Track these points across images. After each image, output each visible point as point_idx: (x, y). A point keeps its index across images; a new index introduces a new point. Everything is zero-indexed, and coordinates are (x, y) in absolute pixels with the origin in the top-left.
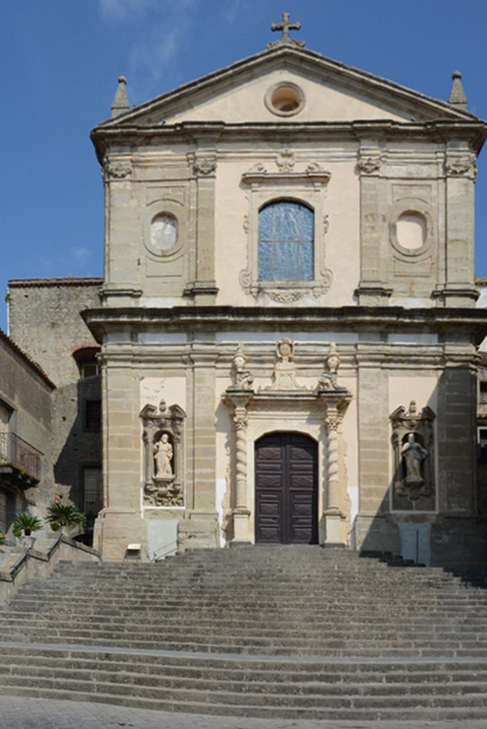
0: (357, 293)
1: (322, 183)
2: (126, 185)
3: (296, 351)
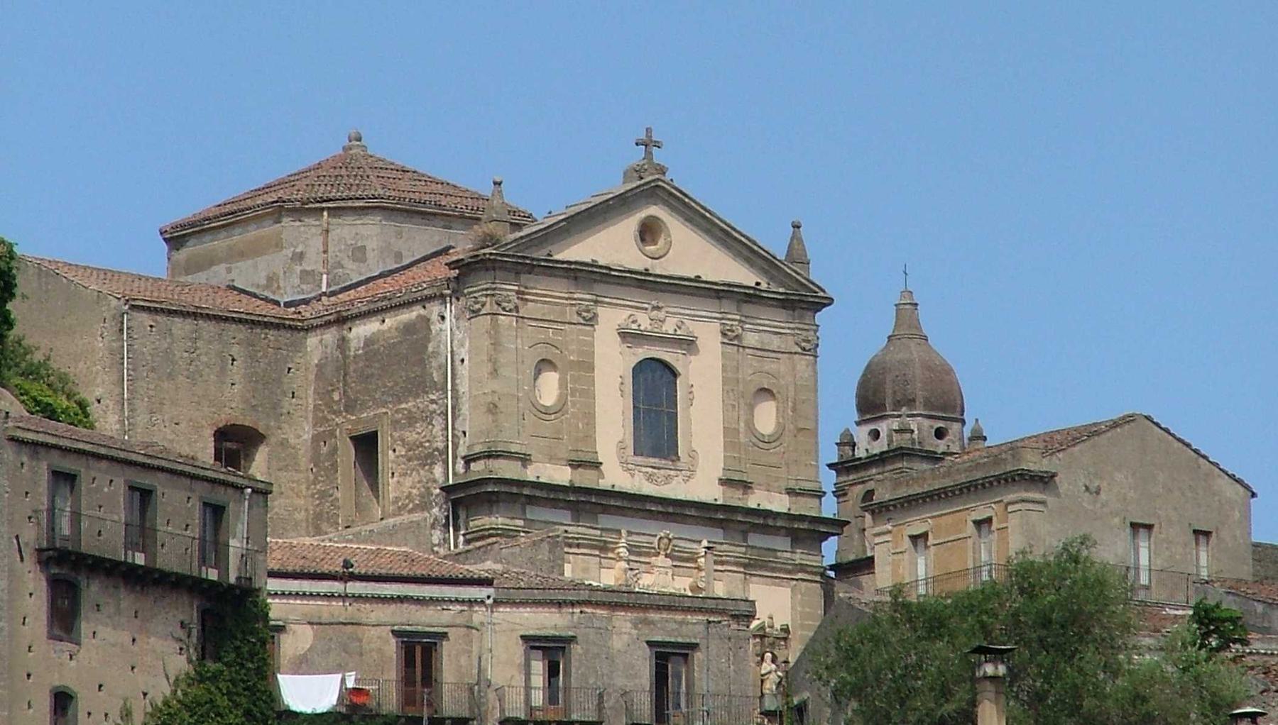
0: (726, 482)
1: (688, 345)
2: (513, 321)
3: (674, 546)
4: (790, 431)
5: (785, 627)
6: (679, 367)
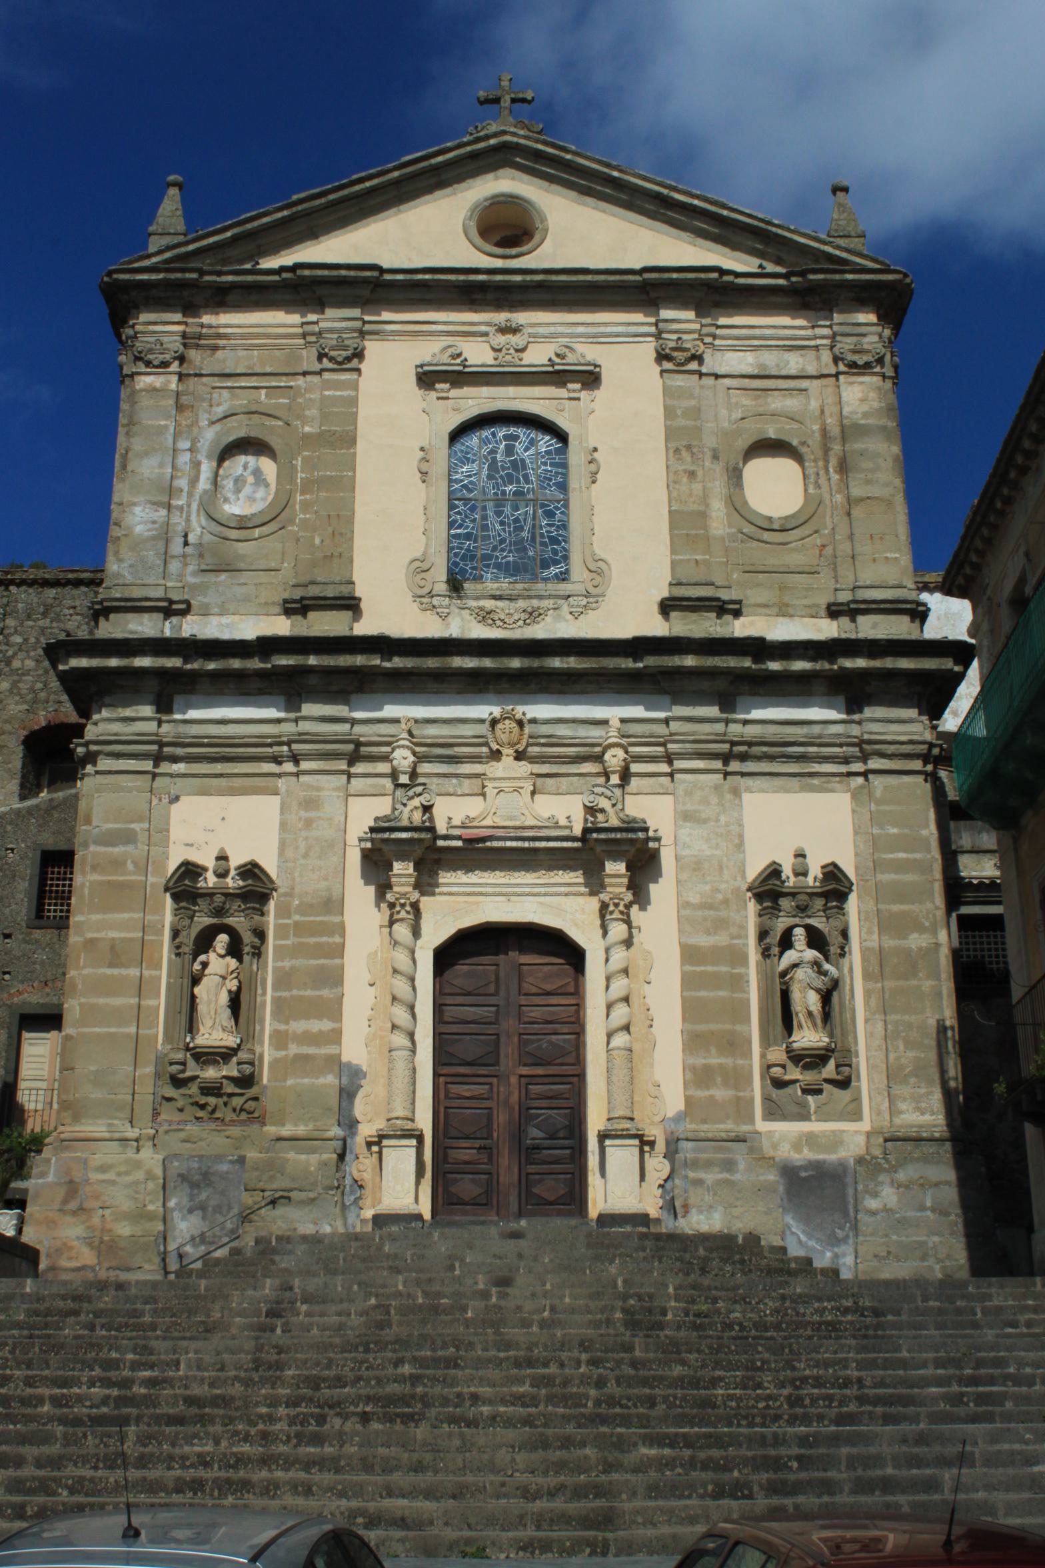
0: (667, 607)
5: (831, 868)
6: (563, 422)
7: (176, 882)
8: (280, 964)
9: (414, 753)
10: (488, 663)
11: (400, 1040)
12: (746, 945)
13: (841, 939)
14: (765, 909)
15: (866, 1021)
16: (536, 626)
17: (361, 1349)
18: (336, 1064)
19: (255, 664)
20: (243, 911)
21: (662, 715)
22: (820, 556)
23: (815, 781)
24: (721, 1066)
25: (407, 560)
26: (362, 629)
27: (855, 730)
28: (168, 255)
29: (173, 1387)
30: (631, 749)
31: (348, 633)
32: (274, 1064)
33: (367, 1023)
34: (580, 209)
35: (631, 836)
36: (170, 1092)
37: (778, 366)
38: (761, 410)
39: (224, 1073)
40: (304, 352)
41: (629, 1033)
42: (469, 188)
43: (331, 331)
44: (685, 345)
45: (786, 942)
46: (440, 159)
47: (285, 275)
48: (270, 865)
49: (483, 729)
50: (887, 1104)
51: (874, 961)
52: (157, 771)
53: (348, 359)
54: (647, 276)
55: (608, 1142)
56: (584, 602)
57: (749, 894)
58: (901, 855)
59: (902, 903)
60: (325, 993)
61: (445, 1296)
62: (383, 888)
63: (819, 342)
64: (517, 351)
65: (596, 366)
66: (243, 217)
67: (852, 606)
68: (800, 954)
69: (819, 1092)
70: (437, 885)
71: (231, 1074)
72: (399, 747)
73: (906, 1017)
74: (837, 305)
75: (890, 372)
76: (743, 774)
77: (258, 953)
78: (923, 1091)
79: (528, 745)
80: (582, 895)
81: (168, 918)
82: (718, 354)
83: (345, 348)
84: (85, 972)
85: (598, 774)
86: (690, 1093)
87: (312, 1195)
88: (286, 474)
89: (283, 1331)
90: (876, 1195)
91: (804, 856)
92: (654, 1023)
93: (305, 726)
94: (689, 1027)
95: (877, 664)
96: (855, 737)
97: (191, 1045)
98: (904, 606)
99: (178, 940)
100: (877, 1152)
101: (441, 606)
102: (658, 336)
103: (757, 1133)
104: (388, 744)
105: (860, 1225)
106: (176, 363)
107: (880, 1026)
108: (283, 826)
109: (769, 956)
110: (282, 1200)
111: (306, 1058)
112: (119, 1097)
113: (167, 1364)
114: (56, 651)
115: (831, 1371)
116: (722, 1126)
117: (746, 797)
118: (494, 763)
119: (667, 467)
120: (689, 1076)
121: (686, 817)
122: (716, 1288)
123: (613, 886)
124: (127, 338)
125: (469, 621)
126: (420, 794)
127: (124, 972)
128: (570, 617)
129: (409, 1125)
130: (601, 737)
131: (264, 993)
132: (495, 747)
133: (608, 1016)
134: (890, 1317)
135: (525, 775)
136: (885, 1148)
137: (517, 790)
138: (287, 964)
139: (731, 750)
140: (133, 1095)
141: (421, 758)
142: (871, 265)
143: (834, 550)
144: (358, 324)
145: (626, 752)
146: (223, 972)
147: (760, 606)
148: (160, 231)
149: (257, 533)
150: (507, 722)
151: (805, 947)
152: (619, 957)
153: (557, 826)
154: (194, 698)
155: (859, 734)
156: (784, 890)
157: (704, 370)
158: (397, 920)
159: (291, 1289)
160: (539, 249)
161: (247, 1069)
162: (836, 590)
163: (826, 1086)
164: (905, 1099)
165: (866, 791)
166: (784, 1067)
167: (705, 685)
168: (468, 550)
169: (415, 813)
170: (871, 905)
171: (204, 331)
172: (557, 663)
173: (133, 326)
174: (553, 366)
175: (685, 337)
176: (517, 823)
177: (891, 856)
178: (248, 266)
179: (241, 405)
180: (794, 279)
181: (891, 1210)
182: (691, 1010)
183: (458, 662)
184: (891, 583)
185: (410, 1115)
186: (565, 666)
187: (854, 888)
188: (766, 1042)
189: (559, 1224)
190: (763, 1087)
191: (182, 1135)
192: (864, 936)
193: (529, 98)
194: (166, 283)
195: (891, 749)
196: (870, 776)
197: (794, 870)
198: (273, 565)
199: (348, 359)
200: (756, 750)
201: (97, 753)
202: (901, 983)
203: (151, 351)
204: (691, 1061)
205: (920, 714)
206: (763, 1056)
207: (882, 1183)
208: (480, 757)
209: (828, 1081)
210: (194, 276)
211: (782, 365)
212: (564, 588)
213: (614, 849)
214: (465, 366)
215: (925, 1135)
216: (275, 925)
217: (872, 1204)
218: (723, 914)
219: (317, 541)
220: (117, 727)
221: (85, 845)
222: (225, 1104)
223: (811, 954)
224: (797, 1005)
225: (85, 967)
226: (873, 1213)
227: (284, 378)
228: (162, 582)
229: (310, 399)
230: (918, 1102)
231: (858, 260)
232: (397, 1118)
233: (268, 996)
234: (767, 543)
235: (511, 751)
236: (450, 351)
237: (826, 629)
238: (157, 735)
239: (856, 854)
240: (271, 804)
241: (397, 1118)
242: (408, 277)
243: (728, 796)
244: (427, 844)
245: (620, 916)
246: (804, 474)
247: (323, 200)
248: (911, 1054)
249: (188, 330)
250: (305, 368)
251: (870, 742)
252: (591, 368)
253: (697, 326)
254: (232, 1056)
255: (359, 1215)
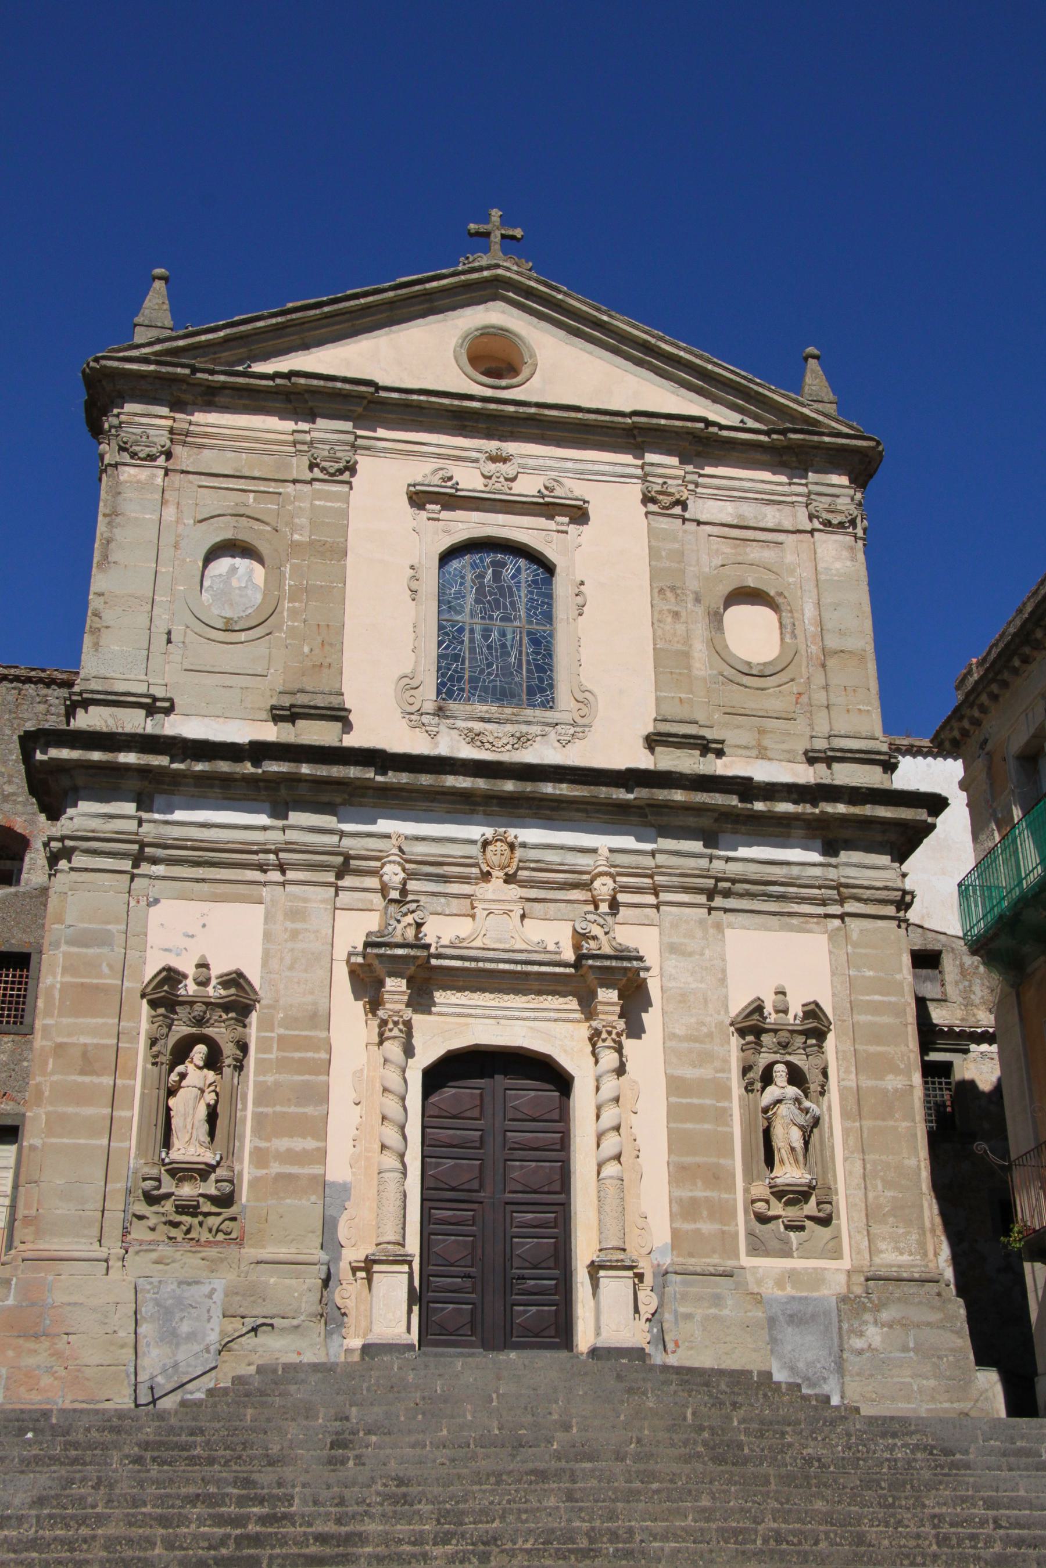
0: (652, 742)
4: (809, 658)
5: (813, 1006)
6: (551, 553)
7: (154, 989)
8: (261, 1078)
9: (404, 870)
10: (481, 783)
11: (390, 1161)
12: (729, 1079)
13: (821, 1077)
14: (748, 1043)
15: (845, 1159)
16: (524, 751)
17: (492, 1480)
18: (321, 1184)
19: (248, 768)
20: (224, 1022)
21: (649, 847)
22: (797, 703)
23: (795, 921)
24: (707, 1199)
25: (397, 676)
26: (350, 741)
27: (832, 874)
28: (158, 348)
29: (294, 1525)
30: (618, 879)
31: (337, 744)
32: (254, 1183)
33: (352, 1143)
34: (568, 348)
35: (626, 964)
36: (141, 1208)
37: (755, 517)
38: (740, 559)
39: (201, 1191)
40: (294, 460)
41: (620, 1162)
42: (458, 317)
43: (323, 442)
44: (669, 490)
45: (767, 1078)
46: (434, 284)
47: (279, 381)
48: (254, 976)
49: (475, 850)
50: (867, 1243)
51: (852, 1100)
52: (136, 871)
53: (341, 472)
54: (636, 419)
55: (602, 1273)
56: (572, 731)
57: (732, 1029)
58: (877, 997)
59: (878, 1044)
60: (309, 1110)
61: (522, 1427)
62: (374, 1004)
63: (795, 499)
64: (507, 479)
65: (585, 502)
66: (236, 318)
67: (830, 753)
68: (782, 1091)
69: (802, 1228)
70: (434, 1004)
71: (208, 1192)
72: (390, 862)
73: (884, 1157)
74: (812, 465)
75: (860, 532)
76: (726, 910)
77: (239, 1067)
78: (901, 1231)
79: (518, 869)
80: (579, 1021)
81: (144, 1026)
82: (700, 501)
83: (337, 460)
84: (55, 1078)
85: (586, 902)
86: (676, 1225)
87: (295, 1322)
88: (274, 578)
89: (355, 1464)
90: (861, 1334)
91: (784, 994)
92: (640, 1155)
93: (292, 835)
94: (675, 1158)
95: (857, 810)
96: (832, 880)
97: (167, 1160)
98: (878, 757)
99: (155, 1049)
100: (858, 1290)
101: (430, 725)
102: (644, 478)
103: (743, 1268)
104: (378, 859)
105: (847, 1365)
106: (163, 457)
107: (859, 1164)
108: (267, 936)
109: (752, 1091)
110: (264, 1328)
111: (290, 1177)
112: (88, 1213)
113: (279, 1500)
114: (30, 741)
115: (959, 1510)
116: (708, 1260)
117: (728, 932)
118: (483, 885)
119: (652, 606)
120: (676, 1208)
121: (673, 949)
122: (778, 1423)
123: (606, 1013)
124: (111, 427)
125: (458, 741)
126: (413, 912)
127: (95, 1079)
128: (558, 744)
129: (399, 1250)
130: (588, 865)
131: (245, 1109)
132: (485, 869)
133: (598, 1146)
134: (958, 1456)
135: (515, 898)
136: (867, 1286)
137: (507, 913)
138: (270, 1079)
139: (716, 885)
140: (103, 1212)
141: (411, 876)
142: (845, 430)
143: (810, 699)
144: (351, 438)
145: (615, 882)
146: (201, 1085)
147: (739, 747)
148: (147, 323)
149: (243, 637)
150: (499, 844)
151: (785, 1084)
152: (610, 1085)
153: (546, 952)
154: (176, 799)
155: (835, 878)
156: (766, 1026)
157: (687, 515)
158: (388, 1038)
159: (347, 1419)
160: (528, 384)
161: (227, 1187)
162: (812, 737)
163: (808, 1223)
164: (884, 1239)
165: (842, 933)
166: (767, 1202)
167: (691, 821)
168: (455, 671)
169: (408, 929)
170: (848, 1046)
171: (192, 428)
172: (548, 788)
173: (118, 416)
174: (543, 497)
175: (670, 481)
176: (507, 946)
177: (868, 998)
178: (240, 368)
179: (228, 506)
180: (774, 436)
181: (877, 1350)
182: (677, 1142)
183: (452, 781)
184: (864, 735)
185: (400, 1239)
186: (558, 792)
187: (832, 1027)
188: (750, 1177)
189: (563, 1354)
190: (747, 1222)
191: (154, 1256)
192: (842, 1075)
193: (519, 236)
194: (157, 376)
195: (867, 894)
196: (847, 919)
197: (774, 1006)
198: (259, 671)
199: (341, 472)
200: (740, 887)
201: (73, 849)
202: (879, 1123)
203: (136, 443)
204: (678, 1193)
205: (892, 861)
206: (746, 1191)
207: (866, 1322)
208: (469, 878)
209: (809, 1218)
210: (187, 371)
211: (760, 517)
212: (550, 716)
213: (607, 977)
214: (457, 490)
215: (905, 1275)
216: (257, 1038)
217: (858, 1343)
218: (708, 1046)
219: (306, 649)
220: (95, 824)
221: (56, 945)
222: (201, 1224)
223: (792, 1091)
224: (779, 1140)
225: (53, 1073)
226: (860, 1352)
227: (273, 484)
228: (144, 677)
229: (300, 507)
230: (897, 1242)
231: (834, 424)
232: (388, 1243)
233: (249, 1111)
234: (746, 687)
235: (501, 874)
236: (441, 474)
237: (805, 775)
238: (137, 834)
239: (834, 995)
240: (258, 911)
241: (388, 1243)
242: (404, 396)
243: (711, 931)
244: (419, 962)
245: (612, 1044)
246: (781, 623)
247: (318, 312)
248: (890, 1194)
249: (175, 425)
250: (295, 475)
251: (847, 886)
252: (581, 503)
253: (682, 473)
254: (210, 1173)
255: (342, 1345)
